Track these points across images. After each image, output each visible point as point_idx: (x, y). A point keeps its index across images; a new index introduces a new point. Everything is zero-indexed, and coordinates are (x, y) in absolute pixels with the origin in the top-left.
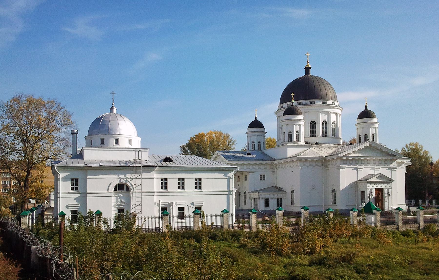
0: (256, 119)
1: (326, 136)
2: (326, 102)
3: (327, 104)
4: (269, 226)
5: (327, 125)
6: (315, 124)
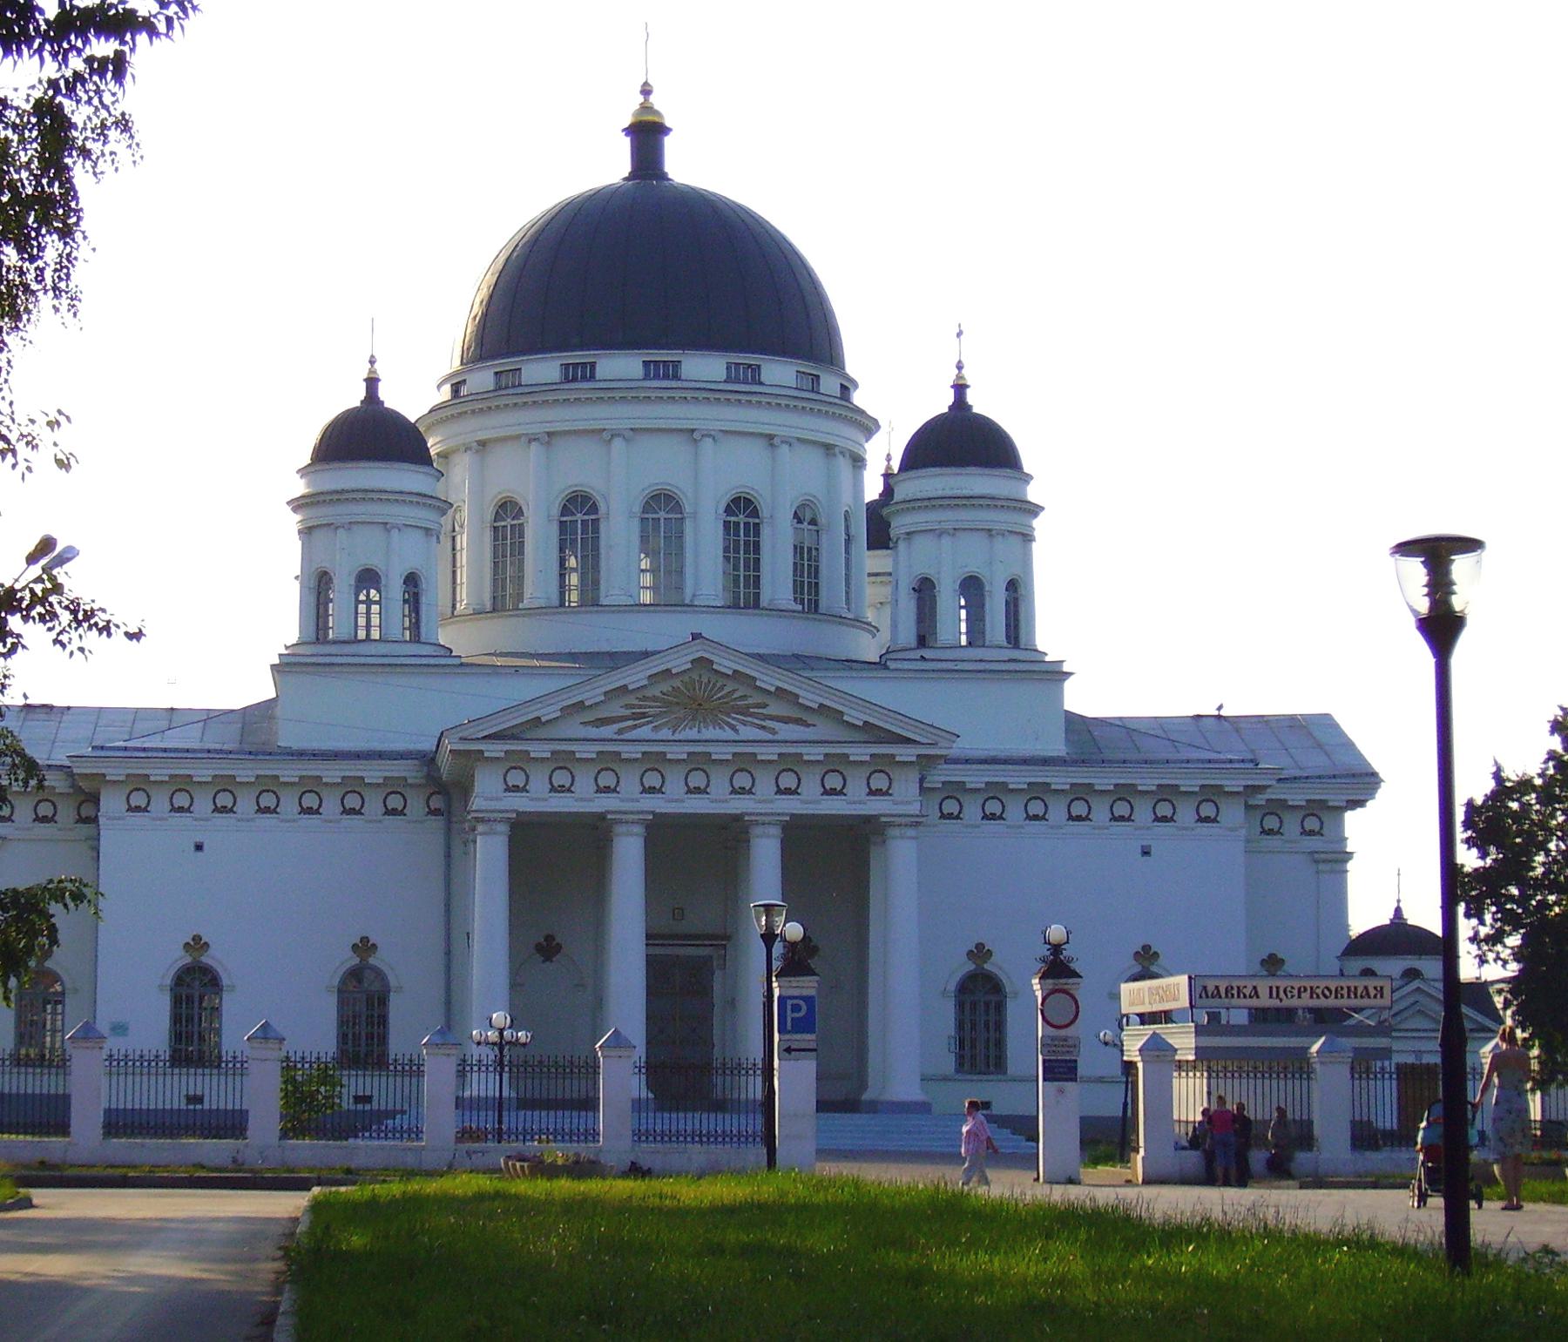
0: (960, 403)
1: (754, 603)
2: (677, 364)
3: (761, 383)
4: (1349, 997)
5: (757, 526)
6: (757, 521)
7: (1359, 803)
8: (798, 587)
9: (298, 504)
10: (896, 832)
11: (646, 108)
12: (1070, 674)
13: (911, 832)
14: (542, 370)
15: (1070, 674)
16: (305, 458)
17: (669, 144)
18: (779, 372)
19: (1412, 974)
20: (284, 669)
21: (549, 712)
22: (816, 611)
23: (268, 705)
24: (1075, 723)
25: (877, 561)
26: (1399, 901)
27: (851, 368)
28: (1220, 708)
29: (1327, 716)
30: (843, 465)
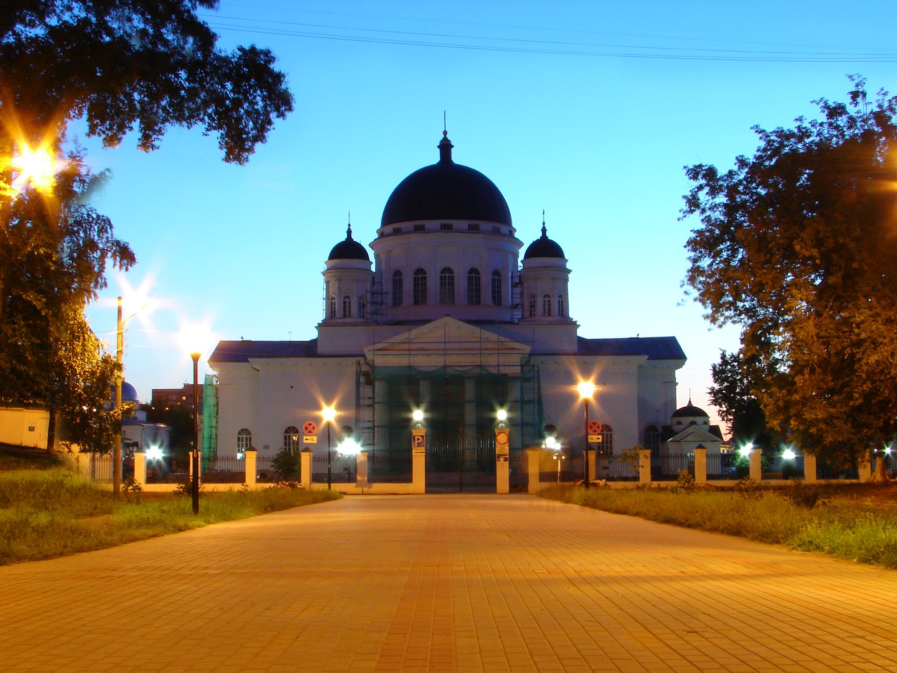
8: (494, 297)
12: (579, 325)
15: (579, 325)
16: (327, 258)
17: (454, 151)
20: (320, 327)
22: (478, 303)
23: (314, 342)
24: (581, 340)
27: (514, 225)
28: (638, 335)
29: (674, 337)
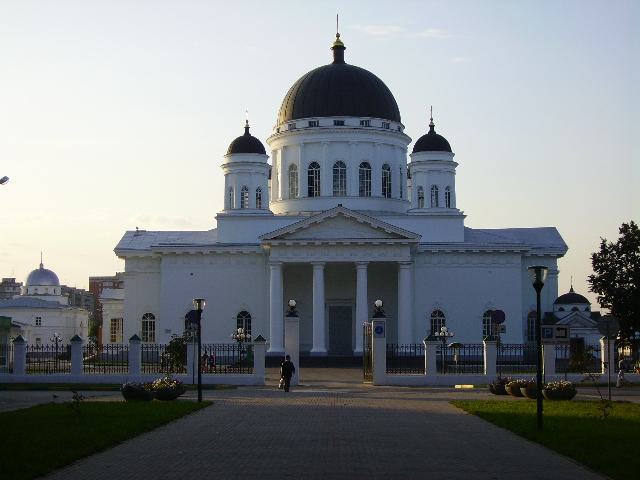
4: (339, 170)
7: (562, 256)
9: (225, 166)
10: (402, 267)
11: (338, 41)
13: (408, 267)
14: (302, 123)
18: (376, 122)
19: (575, 309)
21: (291, 230)
22: (389, 196)
25: (409, 182)
26: (432, 119)
30: (400, 152)
